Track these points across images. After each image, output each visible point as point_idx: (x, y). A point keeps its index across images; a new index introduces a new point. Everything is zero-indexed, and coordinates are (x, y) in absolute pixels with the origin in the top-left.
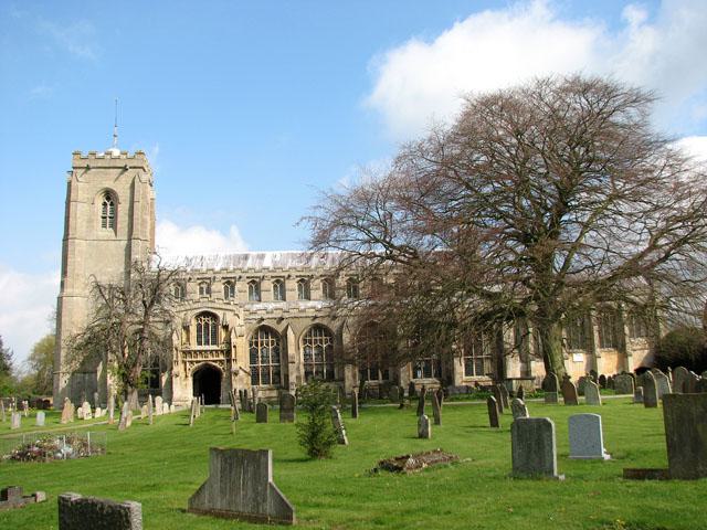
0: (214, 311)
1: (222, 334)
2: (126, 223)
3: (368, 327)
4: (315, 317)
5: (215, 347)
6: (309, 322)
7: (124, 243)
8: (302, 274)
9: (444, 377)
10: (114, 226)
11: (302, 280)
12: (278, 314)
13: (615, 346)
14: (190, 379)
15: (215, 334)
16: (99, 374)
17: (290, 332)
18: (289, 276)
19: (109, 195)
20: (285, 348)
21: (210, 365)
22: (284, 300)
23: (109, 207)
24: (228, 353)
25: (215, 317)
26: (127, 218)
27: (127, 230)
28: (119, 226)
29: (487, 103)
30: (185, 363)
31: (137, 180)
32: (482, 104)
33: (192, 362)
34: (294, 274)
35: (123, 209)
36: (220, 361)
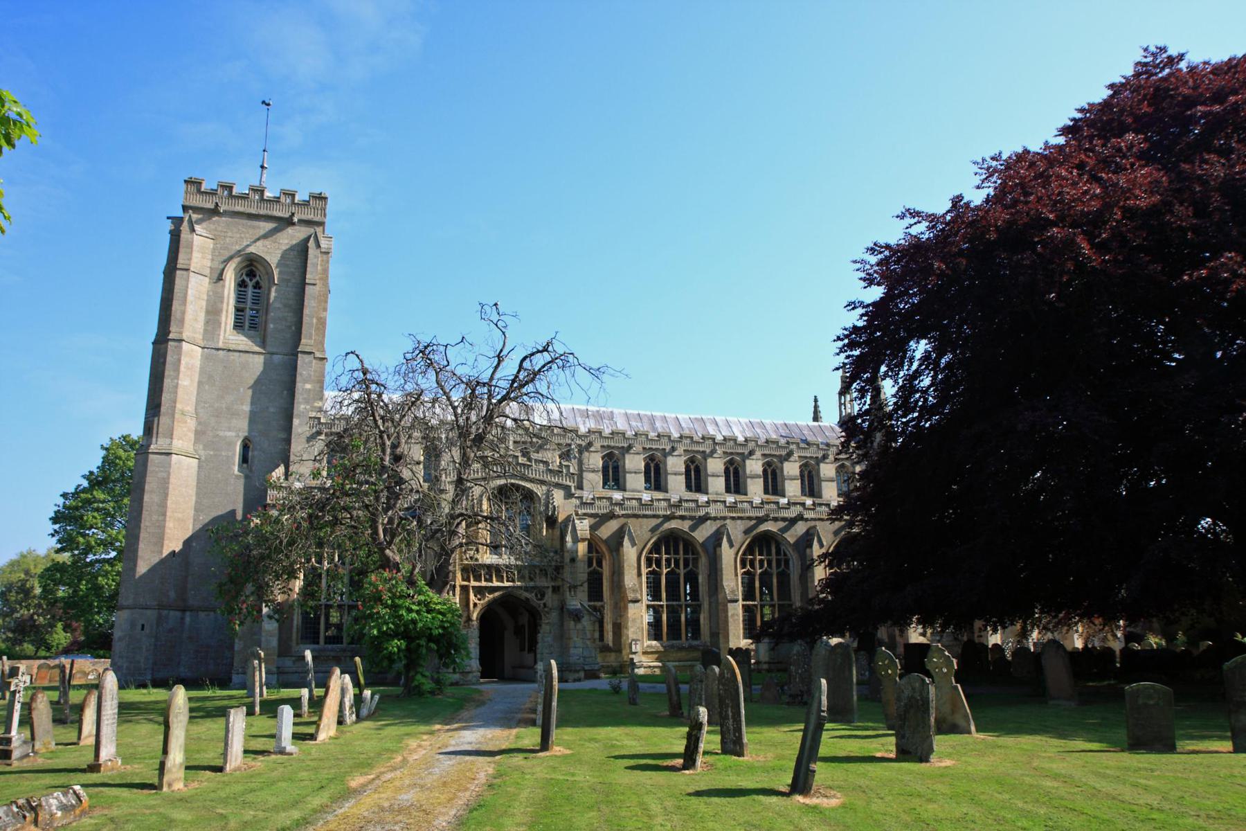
23: (250, 290)
31: (311, 243)
33: (480, 591)
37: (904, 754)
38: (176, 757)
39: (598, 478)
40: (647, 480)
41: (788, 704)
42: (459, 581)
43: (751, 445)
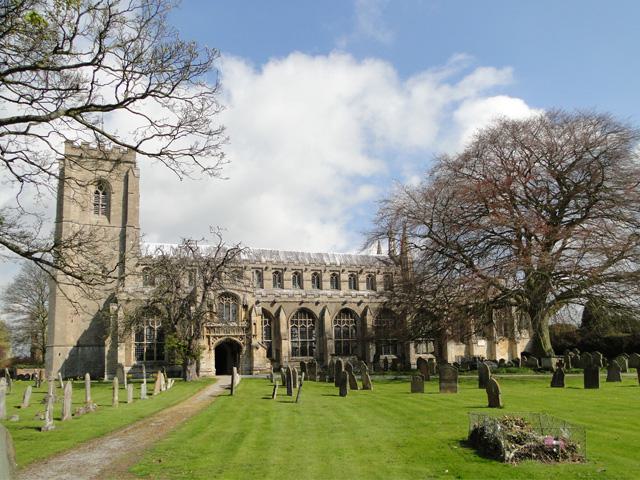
0: (236, 293)
1: (243, 314)
2: (121, 211)
3: (384, 312)
4: (302, 302)
5: (235, 324)
6: (298, 306)
7: (118, 230)
8: (297, 267)
9: (274, 356)
10: (107, 213)
11: (276, 272)
12: (271, 298)
13: (506, 335)
14: (213, 352)
15: (236, 313)
16: (107, 349)
17: (282, 314)
18: (266, 268)
19: (102, 185)
20: (278, 327)
21: (231, 340)
22: (262, 288)
24: (249, 329)
25: (235, 298)
26: (121, 208)
27: (121, 218)
28: (112, 213)
29: (505, 125)
30: (208, 337)
31: (130, 173)
32: (8, 292)
33: (214, 337)
34: (270, 267)
35: (116, 200)
36: (241, 337)
37: (414, 390)
38: (116, 398)
39: (271, 283)
40: (350, 284)
41: (8, 456)
42: (206, 334)
43: (343, 267)
